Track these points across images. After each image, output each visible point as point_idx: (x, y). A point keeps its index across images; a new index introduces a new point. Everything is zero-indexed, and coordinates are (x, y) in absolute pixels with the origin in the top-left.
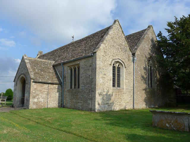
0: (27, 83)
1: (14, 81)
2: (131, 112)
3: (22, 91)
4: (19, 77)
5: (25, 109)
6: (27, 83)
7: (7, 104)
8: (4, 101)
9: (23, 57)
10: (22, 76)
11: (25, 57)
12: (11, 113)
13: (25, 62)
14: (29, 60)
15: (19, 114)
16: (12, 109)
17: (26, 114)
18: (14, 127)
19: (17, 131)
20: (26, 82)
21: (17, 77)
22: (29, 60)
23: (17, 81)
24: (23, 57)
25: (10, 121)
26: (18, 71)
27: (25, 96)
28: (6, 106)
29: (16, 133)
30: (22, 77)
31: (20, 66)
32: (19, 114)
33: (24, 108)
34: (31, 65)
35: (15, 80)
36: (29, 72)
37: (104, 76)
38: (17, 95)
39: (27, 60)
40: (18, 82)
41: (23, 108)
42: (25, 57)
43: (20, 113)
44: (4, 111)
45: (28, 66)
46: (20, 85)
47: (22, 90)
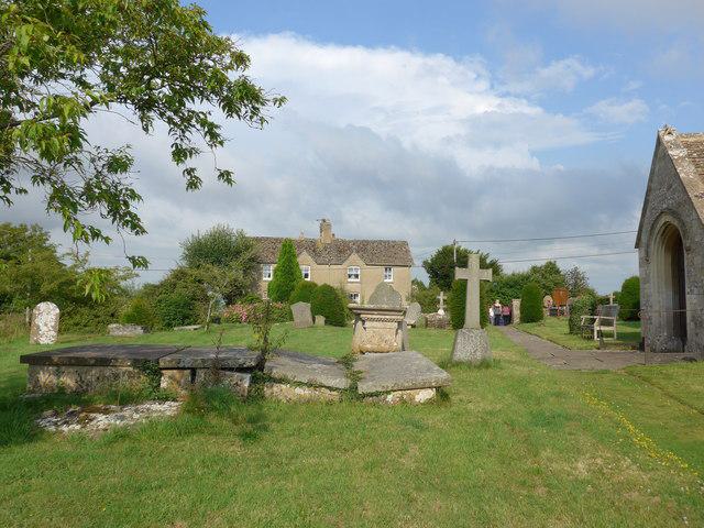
0: (688, 250)
1: (637, 246)
2: (504, 89)
3: (674, 285)
4: (653, 228)
5: (691, 360)
6: (688, 250)
7: (621, 336)
8: (609, 323)
9: (659, 142)
10: (665, 219)
11: (667, 138)
12: (631, 374)
13: (670, 160)
14: (688, 146)
15: (663, 383)
16: (638, 357)
17: (696, 387)
18: (627, 447)
19: (634, 472)
20: (686, 243)
21: (647, 228)
22: (688, 146)
23: (648, 246)
24: (659, 142)
25: (618, 417)
26: (646, 202)
27: (688, 305)
28: (620, 344)
29: (631, 485)
30: (667, 225)
31: (651, 180)
32: (663, 383)
33: (687, 354)
34: (697, 166)
35: (639, 238)
36: (694, 200)
37: (444, 375)
38: (657, 301)
39: (678, 147)
40: (653, 248)
41: (682, 355)
42: (667, 138)
43: (668, 377)
44: (604, 366)
45: (686, 171)
46: (661, 260)
47: (673, 277)
